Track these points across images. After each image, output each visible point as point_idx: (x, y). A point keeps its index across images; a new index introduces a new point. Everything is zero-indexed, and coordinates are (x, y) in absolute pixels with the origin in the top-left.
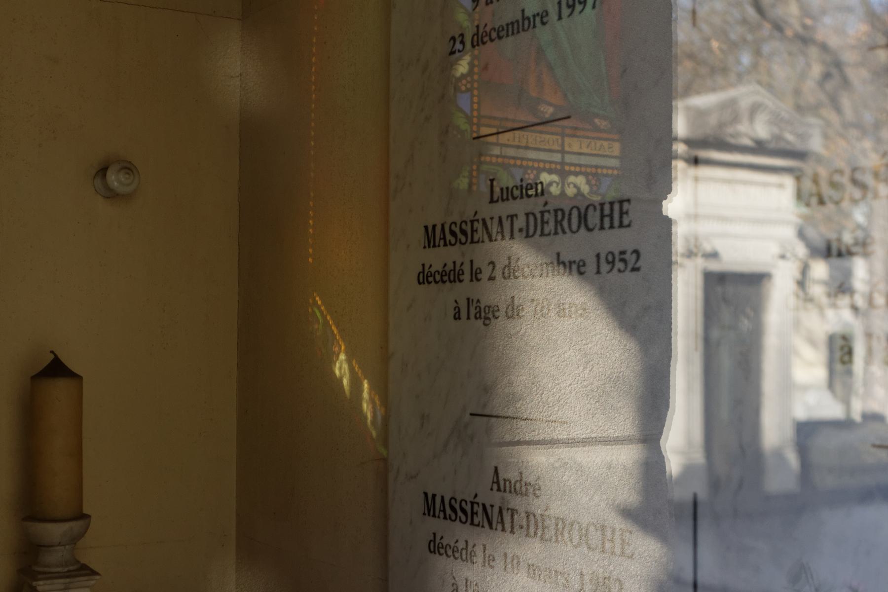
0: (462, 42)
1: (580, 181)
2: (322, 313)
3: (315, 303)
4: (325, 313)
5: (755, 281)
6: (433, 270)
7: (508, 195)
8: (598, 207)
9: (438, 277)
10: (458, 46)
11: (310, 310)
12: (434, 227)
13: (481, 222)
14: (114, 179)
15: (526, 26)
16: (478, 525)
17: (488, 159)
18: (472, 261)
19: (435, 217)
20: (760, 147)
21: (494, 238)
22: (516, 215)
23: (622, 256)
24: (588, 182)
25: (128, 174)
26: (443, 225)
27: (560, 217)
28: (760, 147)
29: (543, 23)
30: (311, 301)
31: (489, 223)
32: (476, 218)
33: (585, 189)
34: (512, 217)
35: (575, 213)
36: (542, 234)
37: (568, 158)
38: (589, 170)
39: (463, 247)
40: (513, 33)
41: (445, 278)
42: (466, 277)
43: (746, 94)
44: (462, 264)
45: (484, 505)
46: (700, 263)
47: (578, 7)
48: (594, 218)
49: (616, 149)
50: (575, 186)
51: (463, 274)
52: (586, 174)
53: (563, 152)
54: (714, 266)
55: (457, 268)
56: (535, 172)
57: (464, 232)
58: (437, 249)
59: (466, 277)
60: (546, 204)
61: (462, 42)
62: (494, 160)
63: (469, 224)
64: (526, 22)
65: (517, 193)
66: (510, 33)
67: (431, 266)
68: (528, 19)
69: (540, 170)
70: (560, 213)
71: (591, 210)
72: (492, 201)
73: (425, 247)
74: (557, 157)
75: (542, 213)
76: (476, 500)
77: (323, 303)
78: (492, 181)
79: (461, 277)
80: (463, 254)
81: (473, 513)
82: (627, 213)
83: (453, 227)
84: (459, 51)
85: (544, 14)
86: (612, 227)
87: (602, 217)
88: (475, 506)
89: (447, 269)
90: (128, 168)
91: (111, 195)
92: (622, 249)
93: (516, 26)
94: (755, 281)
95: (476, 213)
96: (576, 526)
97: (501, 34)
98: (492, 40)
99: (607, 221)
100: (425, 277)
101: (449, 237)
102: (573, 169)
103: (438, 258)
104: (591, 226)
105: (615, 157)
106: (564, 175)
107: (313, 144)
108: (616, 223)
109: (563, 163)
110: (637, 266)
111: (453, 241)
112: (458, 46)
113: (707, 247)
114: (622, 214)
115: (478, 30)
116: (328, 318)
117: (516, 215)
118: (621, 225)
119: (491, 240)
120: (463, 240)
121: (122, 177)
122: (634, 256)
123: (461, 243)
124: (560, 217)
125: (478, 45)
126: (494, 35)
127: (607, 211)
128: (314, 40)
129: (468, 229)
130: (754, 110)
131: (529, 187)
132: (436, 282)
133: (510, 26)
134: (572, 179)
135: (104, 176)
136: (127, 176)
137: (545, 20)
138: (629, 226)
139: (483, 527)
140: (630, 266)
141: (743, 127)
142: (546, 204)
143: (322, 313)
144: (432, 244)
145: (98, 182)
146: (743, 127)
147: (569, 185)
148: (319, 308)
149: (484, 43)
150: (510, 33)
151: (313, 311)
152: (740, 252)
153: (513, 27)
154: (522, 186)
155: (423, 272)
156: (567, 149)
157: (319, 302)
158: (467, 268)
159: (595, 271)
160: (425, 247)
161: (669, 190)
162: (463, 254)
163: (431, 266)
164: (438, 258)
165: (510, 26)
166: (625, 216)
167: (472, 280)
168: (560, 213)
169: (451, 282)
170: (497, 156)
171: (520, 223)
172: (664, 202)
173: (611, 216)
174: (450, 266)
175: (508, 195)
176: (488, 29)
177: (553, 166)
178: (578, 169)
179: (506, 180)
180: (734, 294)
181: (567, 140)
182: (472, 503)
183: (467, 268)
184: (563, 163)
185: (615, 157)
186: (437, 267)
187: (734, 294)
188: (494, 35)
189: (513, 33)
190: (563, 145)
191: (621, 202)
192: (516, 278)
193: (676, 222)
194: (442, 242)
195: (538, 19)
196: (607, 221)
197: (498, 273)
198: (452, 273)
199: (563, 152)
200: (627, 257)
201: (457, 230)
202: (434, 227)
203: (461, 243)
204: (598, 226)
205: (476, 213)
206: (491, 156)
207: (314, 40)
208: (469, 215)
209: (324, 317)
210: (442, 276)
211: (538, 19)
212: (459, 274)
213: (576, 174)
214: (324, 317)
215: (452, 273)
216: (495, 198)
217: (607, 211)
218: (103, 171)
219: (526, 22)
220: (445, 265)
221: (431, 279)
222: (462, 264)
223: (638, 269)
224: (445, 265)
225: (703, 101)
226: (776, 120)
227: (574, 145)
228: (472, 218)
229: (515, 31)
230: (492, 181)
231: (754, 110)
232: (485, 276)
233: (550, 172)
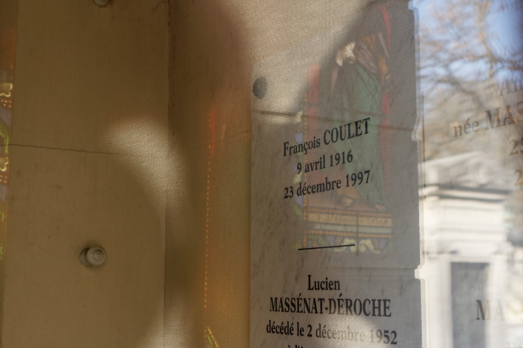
0: (292, 192)
1: (368, 242)
2: (212, 339)
3: (208, 332)
4: (214, 339)
5: (482, 267)
6: (275, 325)
7: (318, 286)
8: (372, 302)
9: (278, 330)
10: (289, 194)
11: (205, 336)
12: (276, 299)
13: (303, 300)
14: (91, 256)
15: (328, 188)
16: (302, 312)
17: (313, 232)
18: (298, 323)
19: (278, 294)
20: (481, 189)
21: (311, 311)
22: (324, 299)
23: (386, 334)
24: (373, 243)
25: (100, 254)
26: (281, 299)
27: (349, 305)
28: (481, 189)
29: (338, 187)
30: (205, 331)
31: (308, 301)
32: (300, 297)
33: (371, 247)
34: (321, 300)
35: (358, 303)
36: (298, 311)
37: (361, 230)
38: (373, 236)
39: (293, 314)
40: (321, 191)
41: (283, 331)
42: (295, 332)
43: (472, 157)
44: (292, 324)
45: (305, 299)
46: (447, 258)
47: (358, 181)
48: (369, 308)
49: (390, 223)
50: (365, 246)
51: (293, 330)
52: (372, 239)
53: (358, 226)
54: (457, 259)
55: (290, 326)
56: (341, 238)
57: (293, 305)
58: (278, 312)
59: (295, 332)
60: (341, 295)
61: (292, 192)
62: (317, 232)
63: (296, 300)
64: (328, 185)
65: (324, 286)
66: (319, 190)
67: (274, 322)
68: (329, 183)
69: (344, 238)
70: (349, 302)
71: (367, 302)
72: (309, 289)
73: (271, 310)
74: (354, 229)
75: (339, 300)
76: (300, 297)
77: (213, 333)
78: (309, 276)
79: (292, 332)
80: (293, 318)
81: (298, 305)
82: (388, 308)
83: (287, 300)
84: (290, 197)
85: (339, 182)
86: (380, 315)
87: (374, 308)
88: (300, 300)
89: (284, 325)
90: (100, 251)
91: (89, 265)
92: (387, 330)
93: (322, 186)
94: (482, 267)
95: (300, 294)
96: (358, 303)
97: (314, 190)
98: (309, 193)
99: (377, 311)
100: (271, 329)
101: (285, 306)
102: (364, 235)
103: (280, 318)
104: (367, 312)
105: (388, 227)
106: (358, 239)
107: (207, 237)
108: (382, 313)
109: (357, 233)
110: (395, 341)
111: (287, 309)
112: (289, 194)
113: (453, 247)
114: (385, 308)
115: (301, 186)
116: (216, 343)
117: (324, 299)
118: (385, 315)
119: (309, 312)
120: (293, 310)
121: (96, 256)
122: (393, 334)
123: (291, 311)
124: (349, 305)
125: (301, 195)
126: (310, 190)
127: (377, 304)
128: (208, 182)
129: (296, 303)
130: (478, 166)
131: (331, 283)
132: (278, 333)
133: (319, 186)
134: (363, 242)
135: (86, 254)
136: (99, 255)
137: (339, 185)
138: (390, 316)
139: (304, 312)
140: (391, 341)
141: (469, 177)
142: (341, 295)
143: (212, 339)
144: (275, 309)
145: (82, 257)
146: (469, 177)
147: (361, 245)
148: (210, 336)
149: (304, 194)
150: (319, 190)
151: (207, 337)
152: (472, 251)
153: (321, 187)
154: (327, 282)
155: (270, 325)
156: (360, 224)
157: (210, 333)
158: (295, 327)
159: (346, 185)
160: (271, 310)
161: (419, 263)
162: (293, 318)
163: (274, 322)
164: (280, 318)
165: (319, 186)
166: (387, 309)
167: (298, 335)
168: (349, 302)
169: (286, 334)
170: (318, 230)
171: (326, 304)
172: (416, 271)
173: (379, 308)
174: (285, 324)
175: (318, 286)
176: (306, 186)
177: (352, 235)
178: (367, 236)
179: (318, 277)
180: (467, 275)
181: (360, 219)
182: (298, 299)
183: (295, 327)
184: (357, 233)
185: (388, 227)
186: (278, 323)
187: (467, 275)
188: (310, 190)
189: (321, 191)
190: (357, 222)
191: (385, 301)
192: (324, 337)
193: (424, 280)
194: (281, 309)
195: (335, 184)
196: (377, 311)
197: (313, 333)
198: (287, 328)
199: (358, 226)
200: (389, 334)
201: (289, 303)
202: (276, 299)
203: (291, 311)
204: (372, 313)
205: (300, 294)
206: (315, 230)
207: (208, 182)
208: (296, 295)
209: (213, 342)
210: (281, 329)
211: (335, 184)
212: (290, 330)
213: (365, 238)
214: (213, 342)
215: (287, 328)
216: (311, 287)
217: (377, 304)
218: (86, 250)
219: (328, 185)
220: (283, 323)
221: (274, 330)
222: (292, 324)
223: (396, 343)
224: (283, 323)
225: (447, 160)
226: (490, 173)
227: (364, 221)
228: (298, 297)
229: (322, 190)
230: (309, 276)
231: (478, 166)
232: (306, 333)
233: (350, 238)
